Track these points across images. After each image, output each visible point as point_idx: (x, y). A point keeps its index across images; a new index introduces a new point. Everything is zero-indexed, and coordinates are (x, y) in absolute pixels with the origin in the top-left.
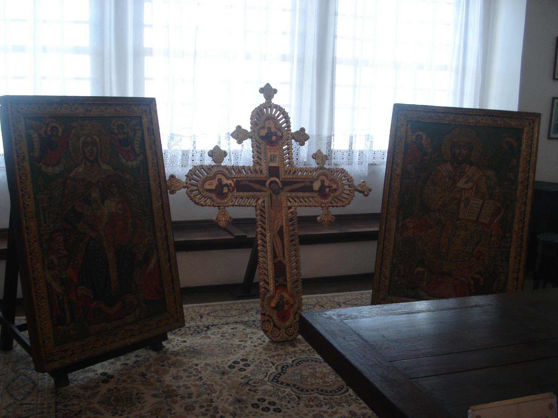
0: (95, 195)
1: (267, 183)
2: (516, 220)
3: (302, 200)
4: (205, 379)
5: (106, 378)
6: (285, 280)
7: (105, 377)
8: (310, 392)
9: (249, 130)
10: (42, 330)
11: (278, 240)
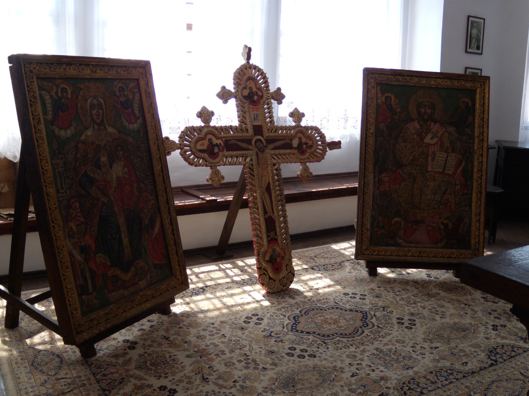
0: (104, 159)
1: (253, 142)
2: (475, 170)
3: (284, 157)
4: (228, 336)
5: (132, 345)
6: (276, 235)
7: (129, 344)
8: (332, 337)
9: (233, 91)
10: (69, 301)
11: (266, 195)
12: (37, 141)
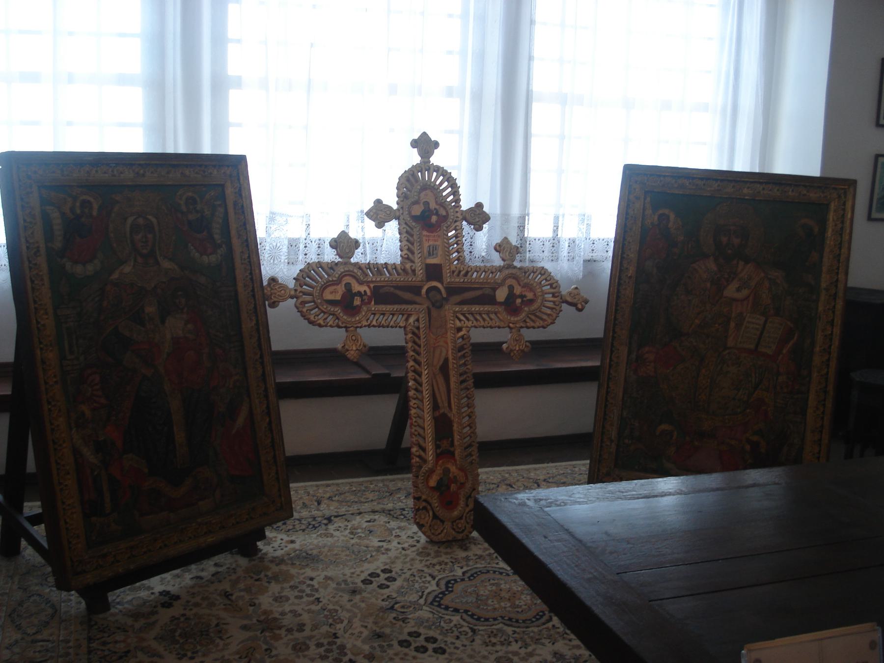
0: (150, 309)
1: (424, 291)
2: (817, 349)
3: (478, 317)
4: (324, 601)
5: (169, 599)
6: (452, 444)
7: (167, 599)
8: (492, 621)
9: (395, 207)
10: (66, 523)
11: (441, 380)
12: (32, 282)
